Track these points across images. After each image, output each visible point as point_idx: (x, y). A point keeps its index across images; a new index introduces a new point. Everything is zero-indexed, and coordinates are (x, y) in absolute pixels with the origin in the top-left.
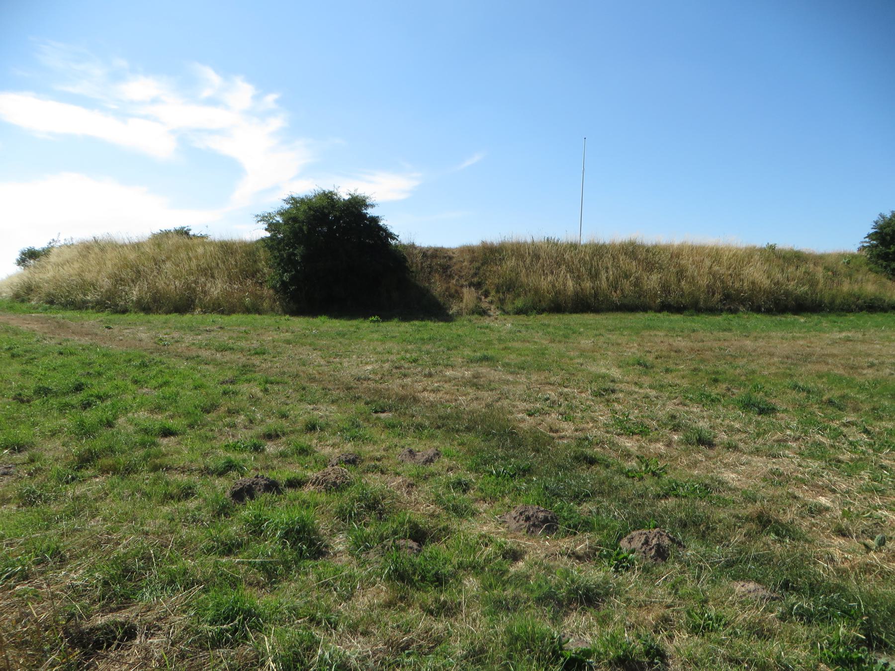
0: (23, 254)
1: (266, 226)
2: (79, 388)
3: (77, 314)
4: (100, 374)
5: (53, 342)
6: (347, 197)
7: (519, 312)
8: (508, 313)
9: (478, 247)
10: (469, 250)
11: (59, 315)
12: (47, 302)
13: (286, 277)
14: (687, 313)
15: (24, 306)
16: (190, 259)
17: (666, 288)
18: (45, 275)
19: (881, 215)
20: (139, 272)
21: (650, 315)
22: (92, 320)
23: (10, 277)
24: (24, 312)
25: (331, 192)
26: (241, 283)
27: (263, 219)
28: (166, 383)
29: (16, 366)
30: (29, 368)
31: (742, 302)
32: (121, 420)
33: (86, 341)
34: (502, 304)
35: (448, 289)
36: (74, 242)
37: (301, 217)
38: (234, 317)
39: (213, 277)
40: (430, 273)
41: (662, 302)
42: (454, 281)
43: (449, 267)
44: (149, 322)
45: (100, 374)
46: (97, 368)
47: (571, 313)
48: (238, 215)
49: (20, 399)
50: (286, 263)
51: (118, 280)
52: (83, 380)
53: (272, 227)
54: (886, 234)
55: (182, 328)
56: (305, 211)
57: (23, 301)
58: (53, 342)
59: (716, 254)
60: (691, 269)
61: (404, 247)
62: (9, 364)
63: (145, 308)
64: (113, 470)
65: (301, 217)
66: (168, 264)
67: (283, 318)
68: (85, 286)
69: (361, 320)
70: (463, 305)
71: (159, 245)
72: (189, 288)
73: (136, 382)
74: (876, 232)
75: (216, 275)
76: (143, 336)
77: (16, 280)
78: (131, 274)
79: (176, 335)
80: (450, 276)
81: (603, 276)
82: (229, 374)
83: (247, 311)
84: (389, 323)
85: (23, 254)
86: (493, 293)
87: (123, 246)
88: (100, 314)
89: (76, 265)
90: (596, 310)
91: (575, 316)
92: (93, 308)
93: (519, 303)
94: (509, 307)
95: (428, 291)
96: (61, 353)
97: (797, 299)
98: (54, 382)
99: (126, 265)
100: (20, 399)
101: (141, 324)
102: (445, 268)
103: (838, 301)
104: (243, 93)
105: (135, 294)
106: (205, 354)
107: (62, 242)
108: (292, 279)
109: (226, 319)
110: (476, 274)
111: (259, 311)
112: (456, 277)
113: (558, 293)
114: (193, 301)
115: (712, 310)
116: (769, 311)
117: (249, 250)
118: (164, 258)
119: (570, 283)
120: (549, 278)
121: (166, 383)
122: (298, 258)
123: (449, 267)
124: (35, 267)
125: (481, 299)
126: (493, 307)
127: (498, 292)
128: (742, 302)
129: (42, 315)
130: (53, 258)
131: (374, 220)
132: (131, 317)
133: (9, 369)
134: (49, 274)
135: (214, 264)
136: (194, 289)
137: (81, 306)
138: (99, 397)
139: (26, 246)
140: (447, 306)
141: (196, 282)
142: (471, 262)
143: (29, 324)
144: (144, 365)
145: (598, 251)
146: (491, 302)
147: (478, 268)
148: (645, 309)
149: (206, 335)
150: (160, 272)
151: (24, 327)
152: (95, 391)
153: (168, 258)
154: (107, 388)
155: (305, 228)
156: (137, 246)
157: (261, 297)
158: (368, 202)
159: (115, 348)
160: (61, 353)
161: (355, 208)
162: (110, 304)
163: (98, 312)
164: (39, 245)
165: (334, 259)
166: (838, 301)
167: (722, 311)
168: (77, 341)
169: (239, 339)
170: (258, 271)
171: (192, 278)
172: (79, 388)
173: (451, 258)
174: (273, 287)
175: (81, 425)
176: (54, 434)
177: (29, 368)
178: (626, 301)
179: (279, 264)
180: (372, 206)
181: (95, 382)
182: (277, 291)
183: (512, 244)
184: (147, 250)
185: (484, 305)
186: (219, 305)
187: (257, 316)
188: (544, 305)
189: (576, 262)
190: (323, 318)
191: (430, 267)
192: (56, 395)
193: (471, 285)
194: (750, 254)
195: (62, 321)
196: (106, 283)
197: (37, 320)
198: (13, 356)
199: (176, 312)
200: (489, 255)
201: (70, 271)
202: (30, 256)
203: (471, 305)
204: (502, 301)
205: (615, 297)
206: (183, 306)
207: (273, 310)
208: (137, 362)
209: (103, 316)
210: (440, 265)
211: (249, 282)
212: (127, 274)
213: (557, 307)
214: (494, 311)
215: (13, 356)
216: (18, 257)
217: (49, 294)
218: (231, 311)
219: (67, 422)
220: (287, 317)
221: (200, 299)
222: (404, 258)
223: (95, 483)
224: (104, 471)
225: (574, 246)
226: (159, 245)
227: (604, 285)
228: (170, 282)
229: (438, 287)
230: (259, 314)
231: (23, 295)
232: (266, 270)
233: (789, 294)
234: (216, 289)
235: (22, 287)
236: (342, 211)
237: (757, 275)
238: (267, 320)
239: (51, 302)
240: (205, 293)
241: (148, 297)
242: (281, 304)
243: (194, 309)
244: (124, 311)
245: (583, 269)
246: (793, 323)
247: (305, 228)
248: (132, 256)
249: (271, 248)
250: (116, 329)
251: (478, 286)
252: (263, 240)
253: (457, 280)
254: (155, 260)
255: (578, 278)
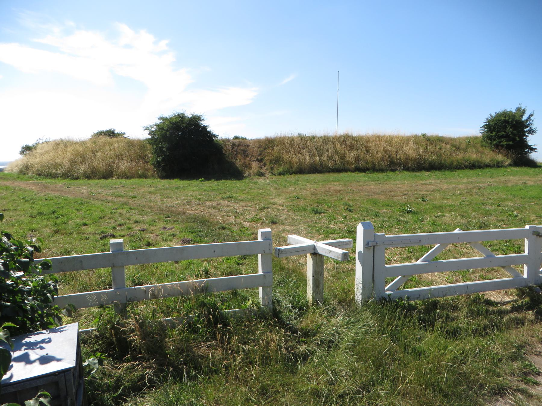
0: (23, 148)
1: (149, 132)
2: (54, 212)
3: (53, 181)
4: (63, 207)
5: (43, 194)
6: (190, 116)
7: (280, 174)
8: (275, 175)
9: (263, 140)
10: (259, 141)
11: (44, 181)
12: (37, 175)
13: (159, 159)
14: (368, 172)
15: (26, 177)
16: (111, 150)
17: (358, 159)
18: (35, 160)
19: (491, 115)
20: (84, 158)
21: (349, 173)
22: (60, 183)
23: (16, 161)
24: (26, 180)
25: (182, 114)
26: (136, 162)
27: (147, 129)
28: (89, 210)
29: (28, 205)
30: (33, 205)
31: (399, 165)
32: (70, 222)
33: (57, 194)
34: (272, 170)
35: (245, 163)
36: (51, 140)
37: (166, 128)
38: (132, 181)
39: (122, 159)
40: (236, 154)
41: (356, 167)
42: (249, 159)
43: (247, 151)
44: (89, 184)
45: (63, 207)
46: (62, 205)
47: (307, 174)
48: (138, 126)
49: (31, 216)
50: (158, 151)
51: (73, 162)
52: (56, 210)
53: (151, 133)
54: (492, 126)
55: (104, 187)
56: (167, 125)
57: (24, 174)
58: (43, 194)
59: (389, 140)
60: (373, 148)
61: (223, 140)
62: (25, 204)
63: (88, 177)
64: (66, 234)
65: (166, 128)
66: (99, 153)
67: (157, 180)
68: (56, 166)
69: (195, 180)
70: (251, 171)
71: (95, 143)
72: (110, 165)
73: (77, 210)
74: (486, 125)
75: (124, 158)
76: (84, 191)
77: (20, 163)
78: (80, 159)
79: (100, 191)
80: (247, 156)
81: (326, 153)
82: (116, 206)
83: (140, 177)
84: (210, 182)
85: (23, 148)
86: (268, 164)
87: (77, 143)
88: (64, 180)
89: (51, 154)
90: (320, 172)
91: (309, 175)
92: (61, 177)
93: (281, 170)
94: (275, 172)
95: (234, 164)
96: (46, 200)
97: (430, 163)
98: (45, 210)
99: (78, 154)
100: (31, 216)
101: (85, 185)
102: (244, 152)
103: (454, 164)
104: (145, 39)
105: (82, 169)
106: (109, 198)
107: (44, 140)
108: (163, 160)
109: (128, 181)
110: (260, 154)
111: (146, 177)
112: (250, 156)
113: (301, 163)
114: (112, 172)
115: (382, 170)
116: (413, 170)
117: (141, 144)
118: (97, 149)
119: (308, 158)
120: (298, 155)
121: (89, 210)
122: (164, 149)
123: (247, 151)
124: (29, 155)
125: (262, 168)
126: (267, 172)
127: (271, 163)
128: (399, 165)
129: (35, 181)
130: (39, 151)
131: (205, 128)
132: (81, 181)
133: (25, 206)
134: (37, 160)
135: (123, 153)
136: (113, 167)
137: (54, 176)
138: (62, 215)
139: (24, 144)
140: (244, 172)
141: (113, 163)
142: (259, 148)
143: (30, 186)
144: (81, 203)
145: (326, 140)
146: (267, 169)
147: (262, 151)
148: (346, 170)
149: (114, 190)
150: (95, 157)
151: (28, 188)
152: (61, 213)
153: (100, 150)
154: (65, 212)
155: (168, 133)
156: (83, 143)
157: (148, 170)
158: (202, 118)
159: (70, 197)
160: (46, 200)
161: (195, 121)
162: (69, 175)
163: (64, 179)
164: (31, 144)
165: (186, 150)
166: (454, 164)
167: (387, 170)
168: (53, 194)
169: (129, 191)
170: (146, 155)
171: (111, 160)
172: (54, 212)
173: (248, 146)
174: (153, 164)
175: (56, 223)
176: (46, 227)
177: (33, 205)
178: (336, 167)
179: (155, 153)
180: (203, 120)
181: (60, 210)
182: (155, 167)
183: (280, 138)
184: (89, 145)
185: (263, 171)
186: (126, 174)
187: (145, 180)
188: (294, 170)
189: (313, 147)
190: (177, 180)
191: (236, 151)
192: (45, 215)
193: (258, 160)
194: (407, 140)
195: (46, 184)
196: (67, 164)
197: (34, 184)
198: (26, 201)
199: (103, 178)
200: (268, 144)
201: (48, 158)
202: (27, 149)
203: (256, 171)
204: (272, 169)
205: (330, 164)
206: (107, 175)
207: (153, 176)
208: (79, 202)
209: (66, 181)
210: (242, 150)
211: (141, 162)
212: (78, 159)
213: (300, 171)
214: (268, 174)
215: (26, 201)
216: (20, 150)
217: (38, 171)
218: (132, 177)
219: (51, 222)
220: (159, 180)
221: (116, 171)
222: (222, 148)
223: (58, 237)
224: (62, 234)
225: (313, 138)
226: (95, 143)
227: (325, 158)
228: (100, 163)
229: (239, 163)
230: (146, 178)
231: (24, 171)
232: (150, 155)
233: (430, 159)
234: (124, 166)
235: (23, 167)
236: (188, 124)
237: (410, 151)
238: (149, 181)
239: (39, 175)
240: (118, 168)
241: (89, 171)
242: (158, 174)
243: (113, 177)
244: (77, 178)
245: (315, 151)
246: (417, 176)
247: (168, 133)
248: (81, 149)
249: (151, 144)
250: (72, 188)
251: (261, 161)
252: (147, 140)
253: (250, 158)
254: (92, 151)
255: (312, 155)
